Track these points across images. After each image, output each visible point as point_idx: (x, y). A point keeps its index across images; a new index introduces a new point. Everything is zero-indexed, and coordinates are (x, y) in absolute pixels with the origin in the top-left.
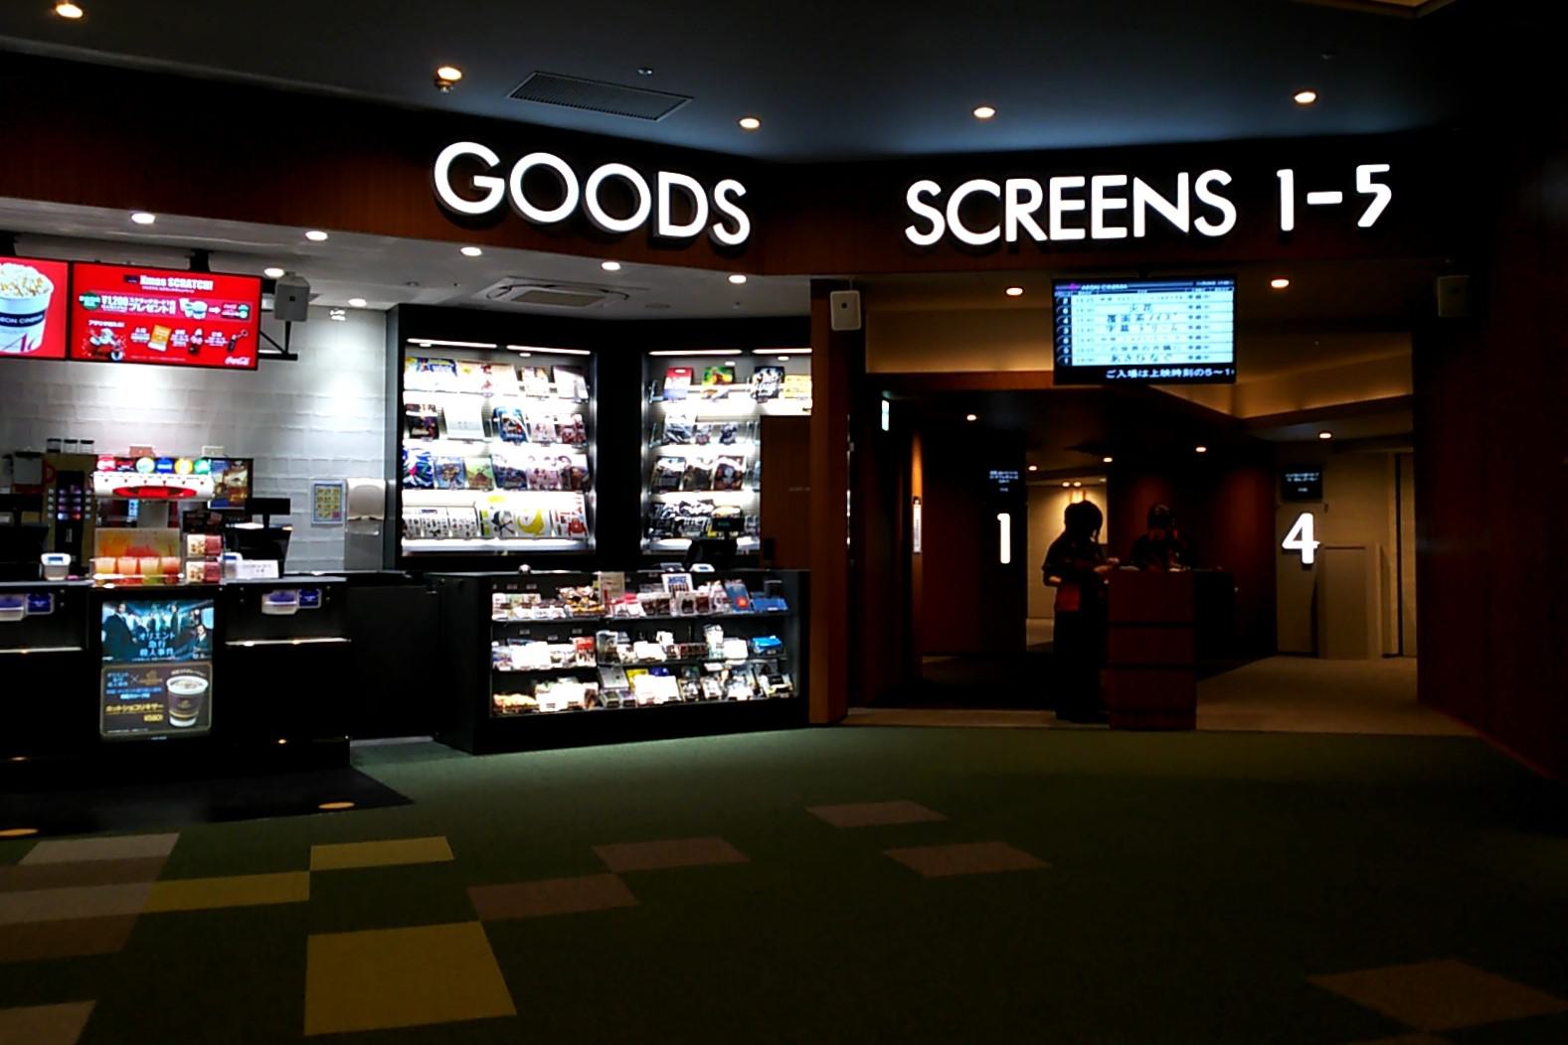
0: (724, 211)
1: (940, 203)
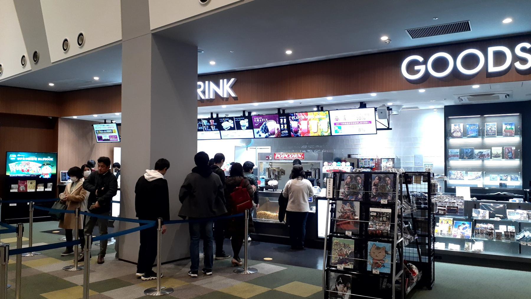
1: (425, 63)
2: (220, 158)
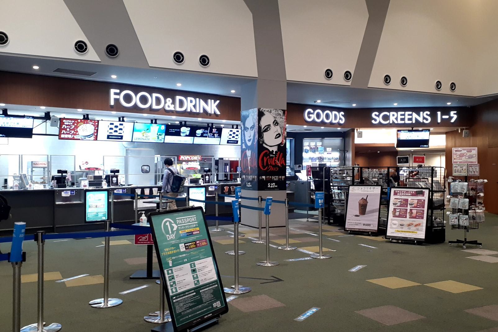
0: (212, 107)
1: (378, 116)
2: (273, 151)
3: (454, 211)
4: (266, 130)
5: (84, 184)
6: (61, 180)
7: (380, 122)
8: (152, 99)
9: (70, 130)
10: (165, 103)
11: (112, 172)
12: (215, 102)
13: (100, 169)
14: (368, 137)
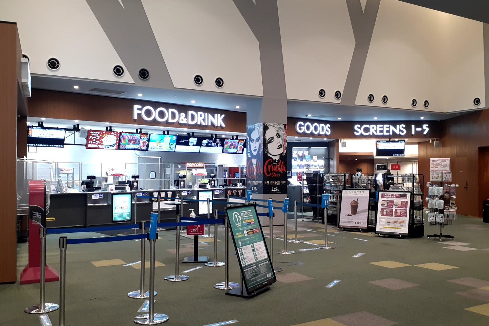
0: (218, 120)
1: (360, 128)
2: (276, 160)
3: (432, 210)
4: (270, 142)
5: (111, 189)
6: (90, 184)
7: (361, 134)
8: (168, 113)
9: (96, 140)
10: (179, 117)
11: (133, 177)
12: (221, 116)
13: (123, 175)
14: (350, 146)
